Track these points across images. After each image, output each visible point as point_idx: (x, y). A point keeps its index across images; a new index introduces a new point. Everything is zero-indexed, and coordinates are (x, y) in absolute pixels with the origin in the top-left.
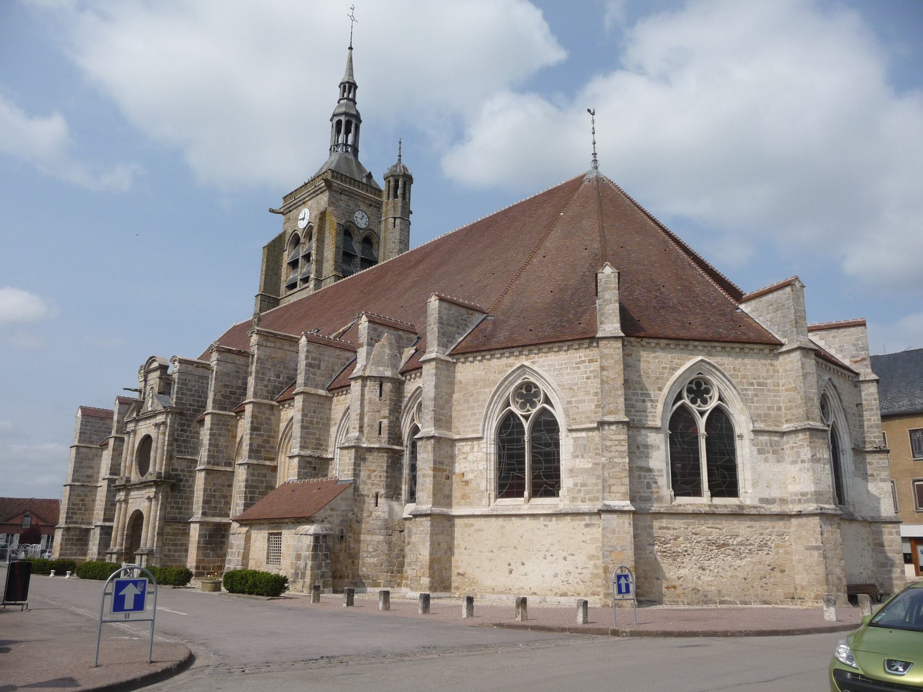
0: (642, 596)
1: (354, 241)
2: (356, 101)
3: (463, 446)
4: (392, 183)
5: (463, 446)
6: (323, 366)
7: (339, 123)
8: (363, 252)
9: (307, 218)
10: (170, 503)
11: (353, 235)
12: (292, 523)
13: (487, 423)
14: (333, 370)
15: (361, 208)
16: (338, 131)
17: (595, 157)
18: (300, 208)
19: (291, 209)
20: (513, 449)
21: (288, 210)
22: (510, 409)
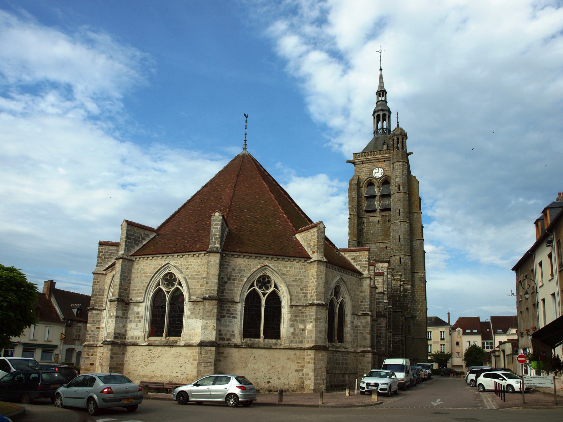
7: (379, 116)
13: (147, 294)
16: (378, 120)
17: (246, 142)
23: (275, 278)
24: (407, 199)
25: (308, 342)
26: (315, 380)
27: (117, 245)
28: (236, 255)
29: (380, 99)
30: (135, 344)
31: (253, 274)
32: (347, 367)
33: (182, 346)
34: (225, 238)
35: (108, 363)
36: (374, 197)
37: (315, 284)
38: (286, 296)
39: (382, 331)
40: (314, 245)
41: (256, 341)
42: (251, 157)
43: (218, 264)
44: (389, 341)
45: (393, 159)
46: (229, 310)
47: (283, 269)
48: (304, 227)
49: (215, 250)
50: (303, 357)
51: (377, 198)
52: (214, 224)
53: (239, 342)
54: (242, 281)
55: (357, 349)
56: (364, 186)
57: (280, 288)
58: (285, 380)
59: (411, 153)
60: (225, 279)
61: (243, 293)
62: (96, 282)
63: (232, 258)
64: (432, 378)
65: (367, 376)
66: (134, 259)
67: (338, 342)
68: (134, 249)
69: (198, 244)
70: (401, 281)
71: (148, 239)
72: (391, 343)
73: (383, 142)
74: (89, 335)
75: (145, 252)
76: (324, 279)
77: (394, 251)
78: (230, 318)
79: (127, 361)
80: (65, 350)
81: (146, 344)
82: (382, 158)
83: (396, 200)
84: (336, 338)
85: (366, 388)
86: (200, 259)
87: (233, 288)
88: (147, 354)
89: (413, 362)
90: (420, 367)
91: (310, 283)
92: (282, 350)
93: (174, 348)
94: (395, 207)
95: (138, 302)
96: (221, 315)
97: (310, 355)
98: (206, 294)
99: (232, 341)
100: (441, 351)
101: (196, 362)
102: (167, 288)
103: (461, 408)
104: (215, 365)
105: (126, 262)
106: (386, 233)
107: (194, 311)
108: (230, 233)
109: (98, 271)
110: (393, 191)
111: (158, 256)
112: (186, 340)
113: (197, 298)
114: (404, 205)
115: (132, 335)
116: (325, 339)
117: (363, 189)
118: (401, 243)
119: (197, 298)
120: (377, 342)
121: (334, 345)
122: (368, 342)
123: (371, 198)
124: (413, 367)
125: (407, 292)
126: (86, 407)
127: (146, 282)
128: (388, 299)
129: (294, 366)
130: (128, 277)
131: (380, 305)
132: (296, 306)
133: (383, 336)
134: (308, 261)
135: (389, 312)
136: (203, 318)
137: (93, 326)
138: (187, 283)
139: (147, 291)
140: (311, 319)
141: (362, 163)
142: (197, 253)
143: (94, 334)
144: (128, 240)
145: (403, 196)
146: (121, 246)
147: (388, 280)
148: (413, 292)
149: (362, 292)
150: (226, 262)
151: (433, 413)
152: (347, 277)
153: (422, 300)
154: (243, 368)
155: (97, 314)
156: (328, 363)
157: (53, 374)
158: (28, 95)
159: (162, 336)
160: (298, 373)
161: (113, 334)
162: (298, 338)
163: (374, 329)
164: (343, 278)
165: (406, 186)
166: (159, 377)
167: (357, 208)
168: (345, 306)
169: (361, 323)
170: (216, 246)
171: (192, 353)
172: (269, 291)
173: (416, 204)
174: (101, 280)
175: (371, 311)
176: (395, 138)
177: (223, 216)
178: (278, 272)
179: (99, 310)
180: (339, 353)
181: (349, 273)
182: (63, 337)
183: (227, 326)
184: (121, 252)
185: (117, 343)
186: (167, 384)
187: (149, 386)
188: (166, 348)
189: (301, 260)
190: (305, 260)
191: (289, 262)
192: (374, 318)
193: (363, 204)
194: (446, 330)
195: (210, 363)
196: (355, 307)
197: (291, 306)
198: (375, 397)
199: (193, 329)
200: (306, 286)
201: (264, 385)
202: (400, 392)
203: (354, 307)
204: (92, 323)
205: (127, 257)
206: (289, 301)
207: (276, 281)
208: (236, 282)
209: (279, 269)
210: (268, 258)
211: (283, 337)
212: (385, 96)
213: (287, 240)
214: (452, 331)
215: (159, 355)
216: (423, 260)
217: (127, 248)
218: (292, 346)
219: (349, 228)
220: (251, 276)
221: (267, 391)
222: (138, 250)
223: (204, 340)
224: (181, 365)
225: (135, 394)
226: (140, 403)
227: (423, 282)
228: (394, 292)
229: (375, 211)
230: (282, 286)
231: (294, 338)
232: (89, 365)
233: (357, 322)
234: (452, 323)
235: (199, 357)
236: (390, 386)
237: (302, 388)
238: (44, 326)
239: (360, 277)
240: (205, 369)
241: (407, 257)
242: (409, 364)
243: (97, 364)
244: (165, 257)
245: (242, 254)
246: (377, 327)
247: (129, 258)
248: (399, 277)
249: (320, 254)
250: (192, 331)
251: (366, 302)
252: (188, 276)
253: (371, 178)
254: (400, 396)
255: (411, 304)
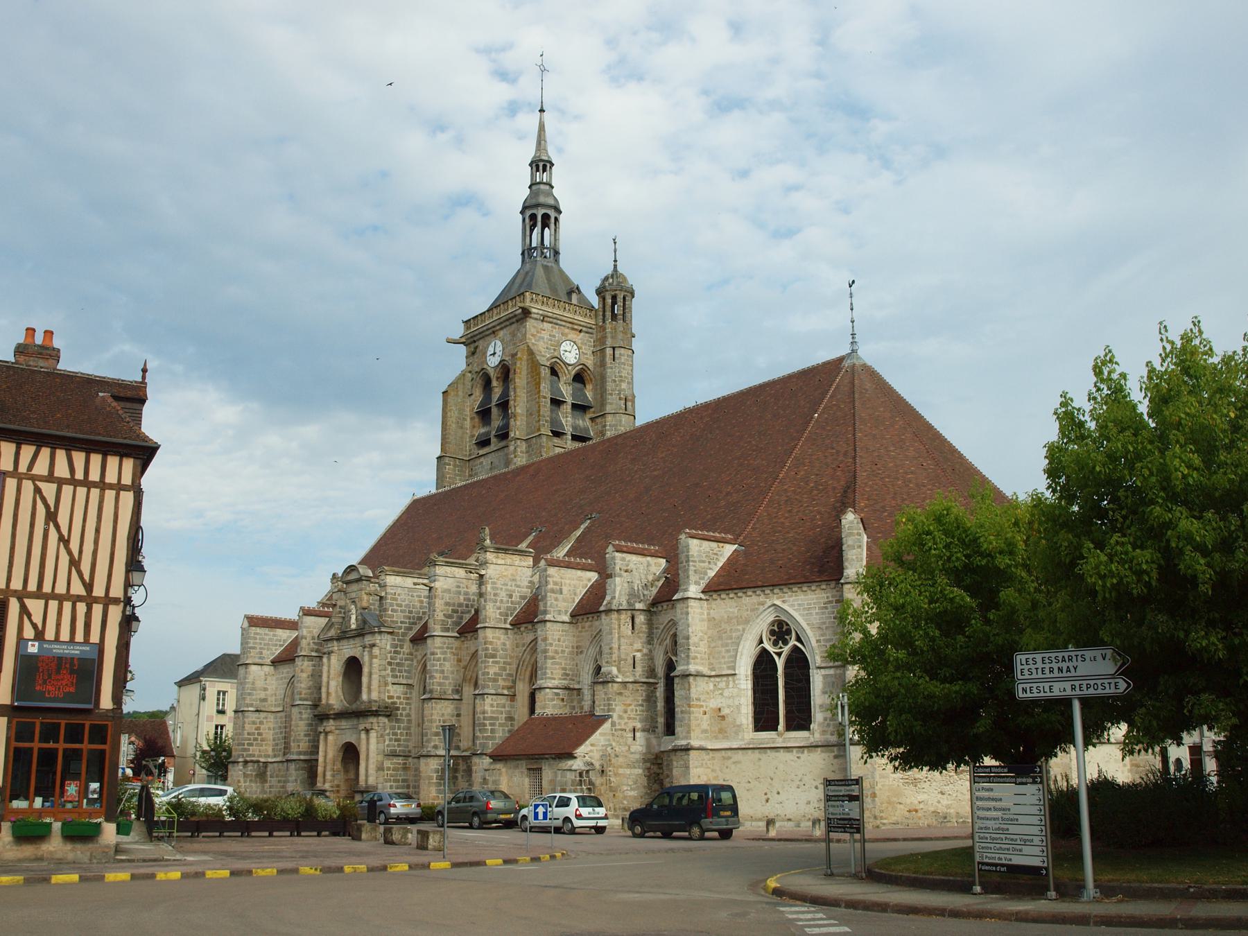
0: (886, 819)
1: (562, 383)
3: (719, 682)
4: (609, 301)
5: (719, 682)
6: (565, 591)
8: (574, 396)
9: (499, 353)
10: (388, 734)
11: (560, 375)
12: (552, 758)
14: (575, 594)
15: (570, 337)
18: (488, 338)
19: (475, 339)
20: (766, 685)
21: (472, 340)
82: (579, 323)
110: (614, 406)
253: (558, 361)
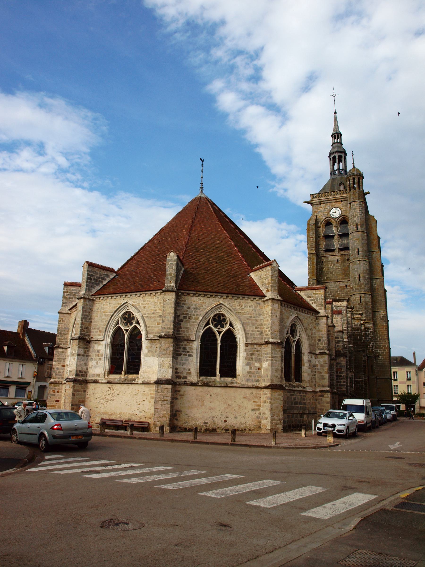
2: (342, 143)
7: (334, 158)
13: (106, 332)
16: (334, 162)
17: (202, 185)
22: (119, 326)
23: (230, 317)
24: (366, 238)
25: (264, 381)
26: (272, 419)
27: (78, 285)
28: (191, 293)
29: (335, 141)
30: (96, 382)
31: (209, 313)
32: (305, 407)
33: (140, 384)
34: (181, 277)
35: (71, 399)
36: (333, 236)
37: (270, 322)
38: (241, 334)
39: (342, 371)
40: (269, 284)
41: (212, 379)
42: (207, 199)
43: (174, 303)
44: (351, 381)
45: (350, 199)
46: (185, 348)
47: (238, 307)
48: (258, 266)
49: (170, 289)
50: (259, 396)
51: (336, 237)
52: (169, 264)
53: (195, 380)
54: (197, 319)
55: (315, 388)
56: (322, 226)
57: (235, 326)
58: (242, 419)
59: (368, 193)
60: (181, 318)
61: (199, 331)
62: (61, 322)
63: (188, 297)
64: (398, 420)
65: (324, 417)
66: (95, 299)
67: (296, 381)
68: (95, 289)
69: (155, 283)
70: (362, 320)
71: (108, 280)
72: (353, 383)
73: (339, 183)
74: (55, 372)
75: (103, 292)
76: (278, 317)
77: (353, 290)
78: (186, 356)
79: (88, 398)
80: (38, 387)
81: (106, 381)
82: (339, 198)
83: (355, 239)
84: (293, 377)
85: (322, 429)
86: (157, 298)
87: (188, 326)
88: (107, 392)
89: (373, 404)
90: (384, 408)
91: (265, 321)
92: (238, 389)
93: (133, 385)
94: (353, 247)
95: (98, 341)
96: (177, 353)
97: (266, 394)
98: (162, 332)
99: (189, 380)
100: (408, 392)
101: (153, 400)
102: (126, 327)
103: (419, 452)
104: (172, 403)
105: (87, 302)
106: (346, 273)
107: (152, 349)
108: (185, 272)
109: (63, 310)
110: (352, 230)
111: (117, 295)
112: (143, 378)
113: (154, 336)
114: (362, 244)
115: (93, 373)
116: (281, 378)
117: (321, 228)
118: (361, 282)
119: (154, 336)
120: (337, 381)
121: (291, 384)
122: (326, 382)
123: (328, 237)
124: (375, 408)
125: (368, 331)
126: (38, 444)
127: (106, 321)
128: (348, 338)
129: (250, 405)
130: (89, 316)
131: (339, 344)
132: (251, 344)
133: (343, 376)
134: (263, 300)
135: (349, 351)
136: (159, 356)
137: (59, 363)
138: (144, 321)
139: (107, 330)
140: (267, 358)
141: (319, 203)
142: (154, 292)
143: (60, 372)
144: (89, 281)
145: (361, 235)
146: (83, 286)
147: (347, 319)
148: (375, 331)
149: (318, 330)
150: (182, 301)
151: (388, 457)
152: (303, 315)
153: (384, 339)
154: (199, 406)
155: (63, 352)
156: (285, 402)
157: (12, 410)
158: (5, 152)
159: (121, 374)
160: (255, 412)
161: (75, 372)
162: (254, 377)
163: (333, 368)
164: (299, 316)
165: (364, 225)
166: (119, 414)
167: (316, 248)
168: (301, 345)
169: (319, 362)
170: (171, 285)
171: (150, 391)
172: (225, 329)
173: (375, 243)
174: (66, 319)
175: (329, 350)
176: (351, 179)
177: (178, 256)
178: (233, 310)
179: (64, 348)
180: (296, 392)
181: (305, 311)
182: (35, 374)
183: (183, 364)
184: (83, 292)
185: (79, 380)
186: (125, 421)
187: (107, 423)
188: (125, 385)
189: (255, 299)
190: (259, 299)
191: (244, 301)
192: (332, 357)
193: (322, 243)
194: (412, 370)
195: (167, 401)
196: (312, 346)
197: (247, 345)
198: (330, 439)
199: (150, 367)
200: (261, 324)
201: (220, 424)
202: (359, 433)
203: (311, 345)
204: (57, 361)
205: (88, 297)
206: (245, 340)
207: (231, 320)
208: (191, 320)
209: (234, 307)
210: (223, 296)
211: (239, 375)
212: (340, 138)
213: (242, 279)
214: (418, 371)
215: (118, 392)
216: (384, 299)
217: (88, 288)
218: (248, 384)
219: (308, 267)
220: (207, 315)
221: (224, 430)
222: (99, 290)
223: (161, 377)
224: (140, 403)
225: (85, 431)
226: (90, 440)
227: (385, 321)
228: (355, 330)
229: (333, 250)
230: (237, 324)
231: (250, 376)
232: (55, 402)
233: (315, 361)
234: (419, 363)
235: (156, 395)
236: (348, 427)
237: (259, 427)
238: (18, 363)
239: (316, 315)
240: (162, 407)
241: (367, 296)
242: (370, 405)
243: (62, 401)
244: (124, 296)
245: (197, 293)
246: (336, 366)
247: (90, 297)
248: (359, 316)
249: (275, 293)
250: (149, 369)
251: (323, 341)
252: (145, 314)
253: (329, 218)
254: (359, 438)
255: (373, 344)
